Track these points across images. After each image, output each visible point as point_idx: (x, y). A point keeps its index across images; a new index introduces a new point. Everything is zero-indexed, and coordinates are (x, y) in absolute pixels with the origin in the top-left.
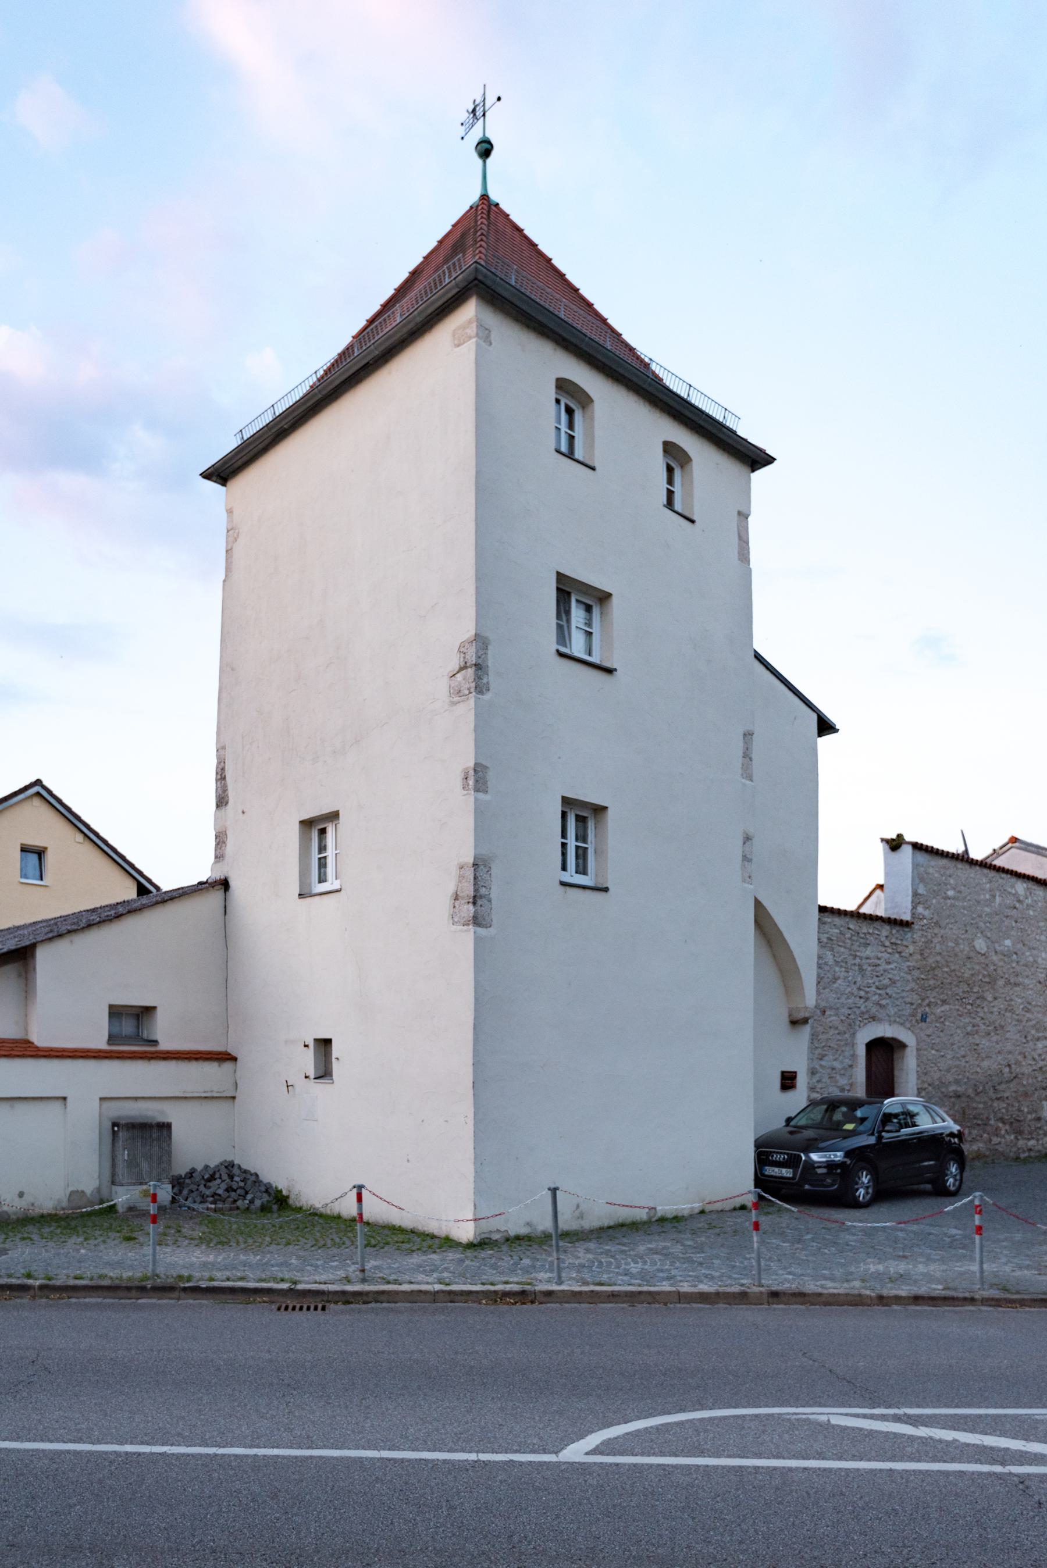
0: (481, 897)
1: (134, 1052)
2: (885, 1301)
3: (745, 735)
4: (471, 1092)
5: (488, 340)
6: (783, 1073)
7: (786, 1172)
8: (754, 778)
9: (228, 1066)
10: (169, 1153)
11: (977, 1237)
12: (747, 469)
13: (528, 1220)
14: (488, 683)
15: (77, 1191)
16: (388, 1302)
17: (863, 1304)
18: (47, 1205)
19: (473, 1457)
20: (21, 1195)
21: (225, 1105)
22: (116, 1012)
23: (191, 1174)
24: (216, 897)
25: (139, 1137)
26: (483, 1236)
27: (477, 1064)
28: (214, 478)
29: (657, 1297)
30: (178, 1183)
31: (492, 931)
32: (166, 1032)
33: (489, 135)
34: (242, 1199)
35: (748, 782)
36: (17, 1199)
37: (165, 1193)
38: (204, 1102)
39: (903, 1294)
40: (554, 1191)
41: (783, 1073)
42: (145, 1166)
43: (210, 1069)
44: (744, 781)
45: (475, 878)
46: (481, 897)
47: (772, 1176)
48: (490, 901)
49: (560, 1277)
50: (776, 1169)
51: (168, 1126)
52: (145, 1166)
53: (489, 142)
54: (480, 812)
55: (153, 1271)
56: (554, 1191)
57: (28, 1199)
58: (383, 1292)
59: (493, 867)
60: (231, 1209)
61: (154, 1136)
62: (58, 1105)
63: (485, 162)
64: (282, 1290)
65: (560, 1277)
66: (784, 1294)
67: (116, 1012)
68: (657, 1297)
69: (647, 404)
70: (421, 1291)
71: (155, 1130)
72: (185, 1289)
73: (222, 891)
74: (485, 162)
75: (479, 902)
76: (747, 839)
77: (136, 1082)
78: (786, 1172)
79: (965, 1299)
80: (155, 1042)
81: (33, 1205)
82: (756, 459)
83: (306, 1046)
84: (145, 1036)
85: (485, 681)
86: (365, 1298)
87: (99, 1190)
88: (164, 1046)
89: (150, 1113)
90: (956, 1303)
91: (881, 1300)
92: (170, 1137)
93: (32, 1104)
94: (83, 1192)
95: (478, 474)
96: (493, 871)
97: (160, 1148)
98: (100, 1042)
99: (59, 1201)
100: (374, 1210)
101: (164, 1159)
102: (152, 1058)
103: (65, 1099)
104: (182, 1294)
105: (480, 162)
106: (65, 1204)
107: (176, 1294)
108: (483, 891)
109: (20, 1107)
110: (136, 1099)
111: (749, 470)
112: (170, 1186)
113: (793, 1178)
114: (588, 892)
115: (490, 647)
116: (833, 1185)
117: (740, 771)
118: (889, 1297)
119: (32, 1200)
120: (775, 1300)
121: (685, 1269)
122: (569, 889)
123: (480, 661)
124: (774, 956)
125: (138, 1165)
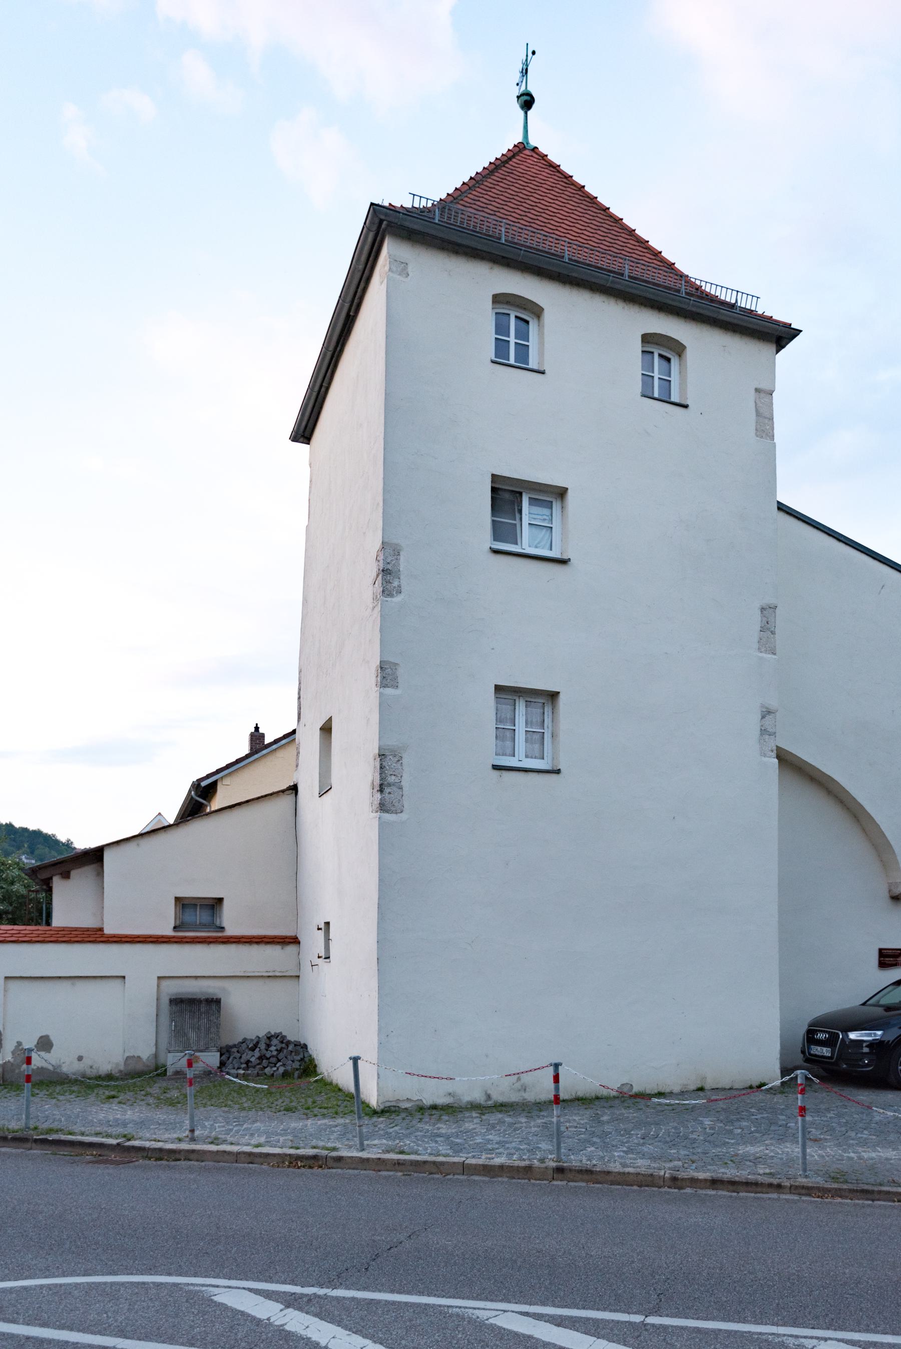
0: (389, 785)
1: (197, 937)
2: (679, 1183)
3: (763, 609)
4: (375, 967)
5: (404, 272)
6: (880, 950)
7: (826, 1051)
8: (778, 651)
9: (291, 949)
10: (218, 1026)
11: (800, 1118)
12: (767, 349)
13: (450, 1091)
14: (399, 586)
15: (134, 1056)
16: (197, 1161)
17: (653, 1185)
18: (105, 1068)
19: (637, 1318)
20: (80, 1058)
21: (295, 981)
22: (182, 903)
23: (244, 1041)
24: (288, 799)
25: (193, 1011)
26: (388, 1104)
27: (381, 942)
28: (301, 440)
29: (441, 1168)
30: (225, 1051)
31: (403, 816)
32: (233, 921)
33: (532, 89)
34: (284, 1065)
35: (774, 657)
36: (76, 1062)
37: (212, 1059)
38: (267, 981)
39: (701, 1175)
40: (355, 1060)
41: (880, 950)
42: (192, 1035)
43: (273, 951)
44: (761, 655)
45: (381, 768)
46: (389, 785)
47: (816, 1056)
48: (401, 788)
49: (362, 1144)
50: (819, 1048)
51: (218, 1002)
52: (192, 1035)
53: (529, 94)
54: (384, 706)
55: (26, 1124)
56: (355, 1060)
57: (87, 1062)
58: (193, 1151)
59: (404, 756)
60: (258, 1075)
61: (203, 1010)
62: (119, 981)
63: (526, 113)
64: (111, 1145)
65: (362, 1144)
66: (570, 1170)
67: (182, 903)
68: (441, 1168)
69: (631, 305)
70: (225, 1152)
71: (203, 1005)
72: (36, 1141)
73: (294, 795)
74: (526, 113)
75: (387, 790)
76: (767, 713)
77: (197, 965)
78: (826, 1051)
79: (771, 1185)
80: (222, 929)
81: (91, 1067)
82: (780, 335)
83: (319, 929)
84: (218, 923)
85: (396, 584)
86: (178, 1156)
87: (156, 1056)
88: (230, 931)
89: (211, 991)
90: (759, 1189)
91: (675, 1182)
92: (219, 1011)
93: (93, 982)
94: (139, 1057)
95: (387, 395)
96: (405, 761)
97: (209, 1020)
98: (169, 932)
99: (117, 1064)
100: (575, 1081)
101: (213, 1030)
102: (211, 942)
103: (124, 977)
104: (34, 1145)
105: (522, 113)
106: (122, 1068)
107: (28, 1145)
108: (392, 779)
109: (80, 984)
110: (196, 977)
111: (773, 348)
112: (219, 1054)
113: (831, 1058)
114: (541, 776)
115: (401, 553)
116: (867, 1065)
117: (756, 646)
118: (683, 1179)
119: (90, 1064)
120: (560, 1176)
121: (398, 1136)
122: (505, 774)
123: (389, 567)
124: (864, 830)
125: (185, 1035)
